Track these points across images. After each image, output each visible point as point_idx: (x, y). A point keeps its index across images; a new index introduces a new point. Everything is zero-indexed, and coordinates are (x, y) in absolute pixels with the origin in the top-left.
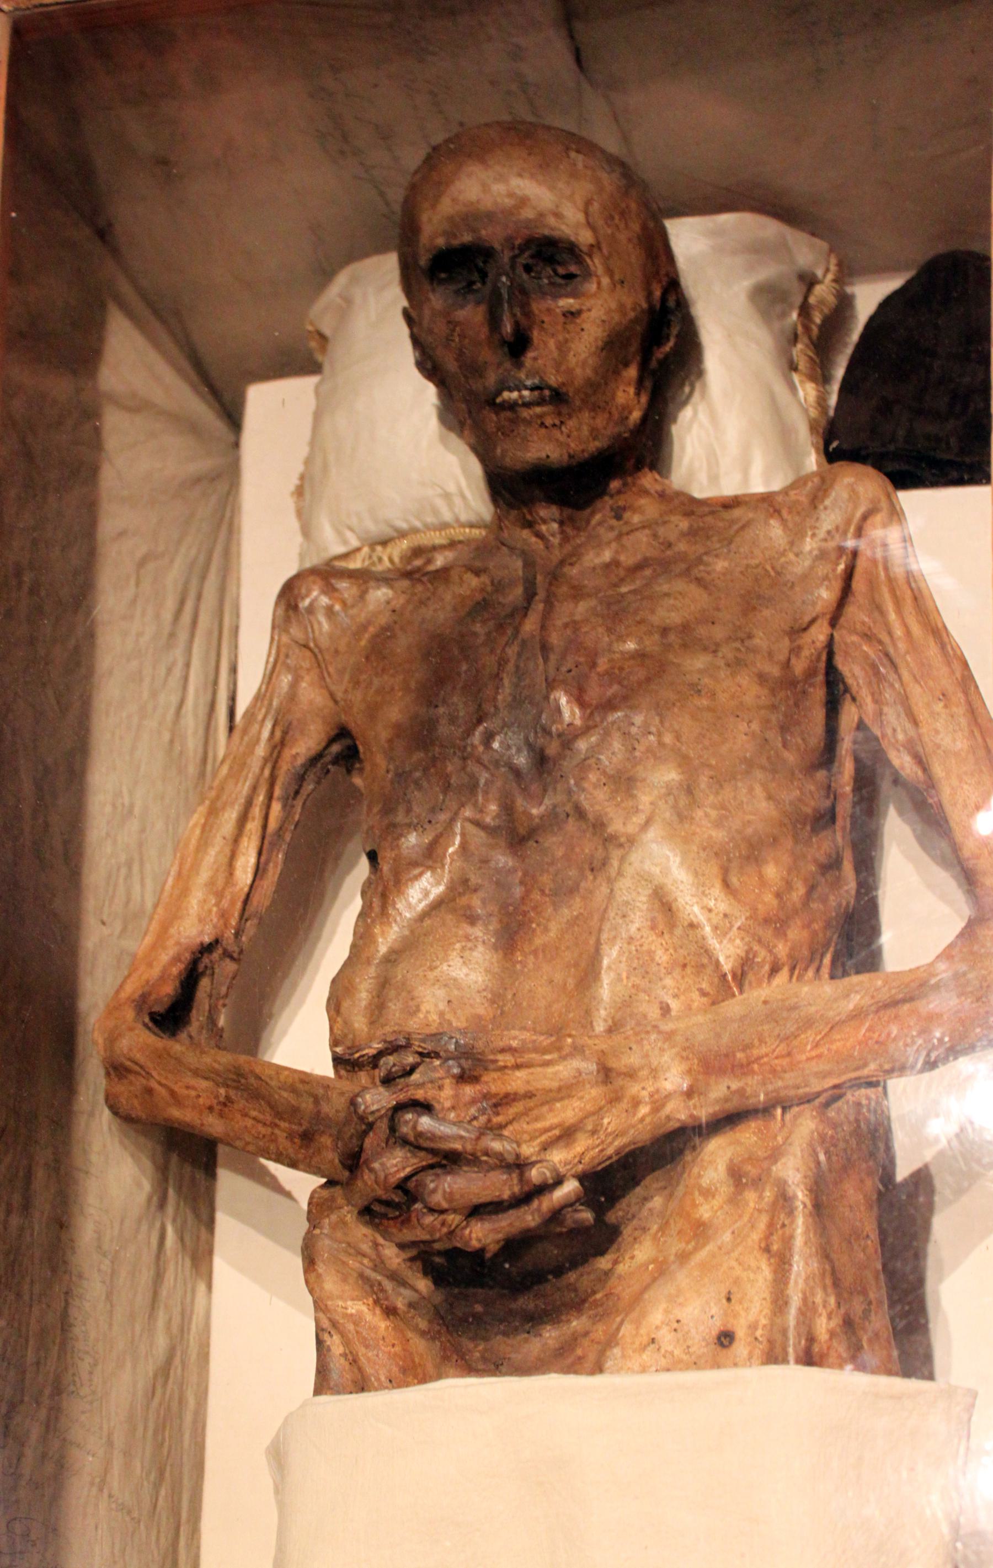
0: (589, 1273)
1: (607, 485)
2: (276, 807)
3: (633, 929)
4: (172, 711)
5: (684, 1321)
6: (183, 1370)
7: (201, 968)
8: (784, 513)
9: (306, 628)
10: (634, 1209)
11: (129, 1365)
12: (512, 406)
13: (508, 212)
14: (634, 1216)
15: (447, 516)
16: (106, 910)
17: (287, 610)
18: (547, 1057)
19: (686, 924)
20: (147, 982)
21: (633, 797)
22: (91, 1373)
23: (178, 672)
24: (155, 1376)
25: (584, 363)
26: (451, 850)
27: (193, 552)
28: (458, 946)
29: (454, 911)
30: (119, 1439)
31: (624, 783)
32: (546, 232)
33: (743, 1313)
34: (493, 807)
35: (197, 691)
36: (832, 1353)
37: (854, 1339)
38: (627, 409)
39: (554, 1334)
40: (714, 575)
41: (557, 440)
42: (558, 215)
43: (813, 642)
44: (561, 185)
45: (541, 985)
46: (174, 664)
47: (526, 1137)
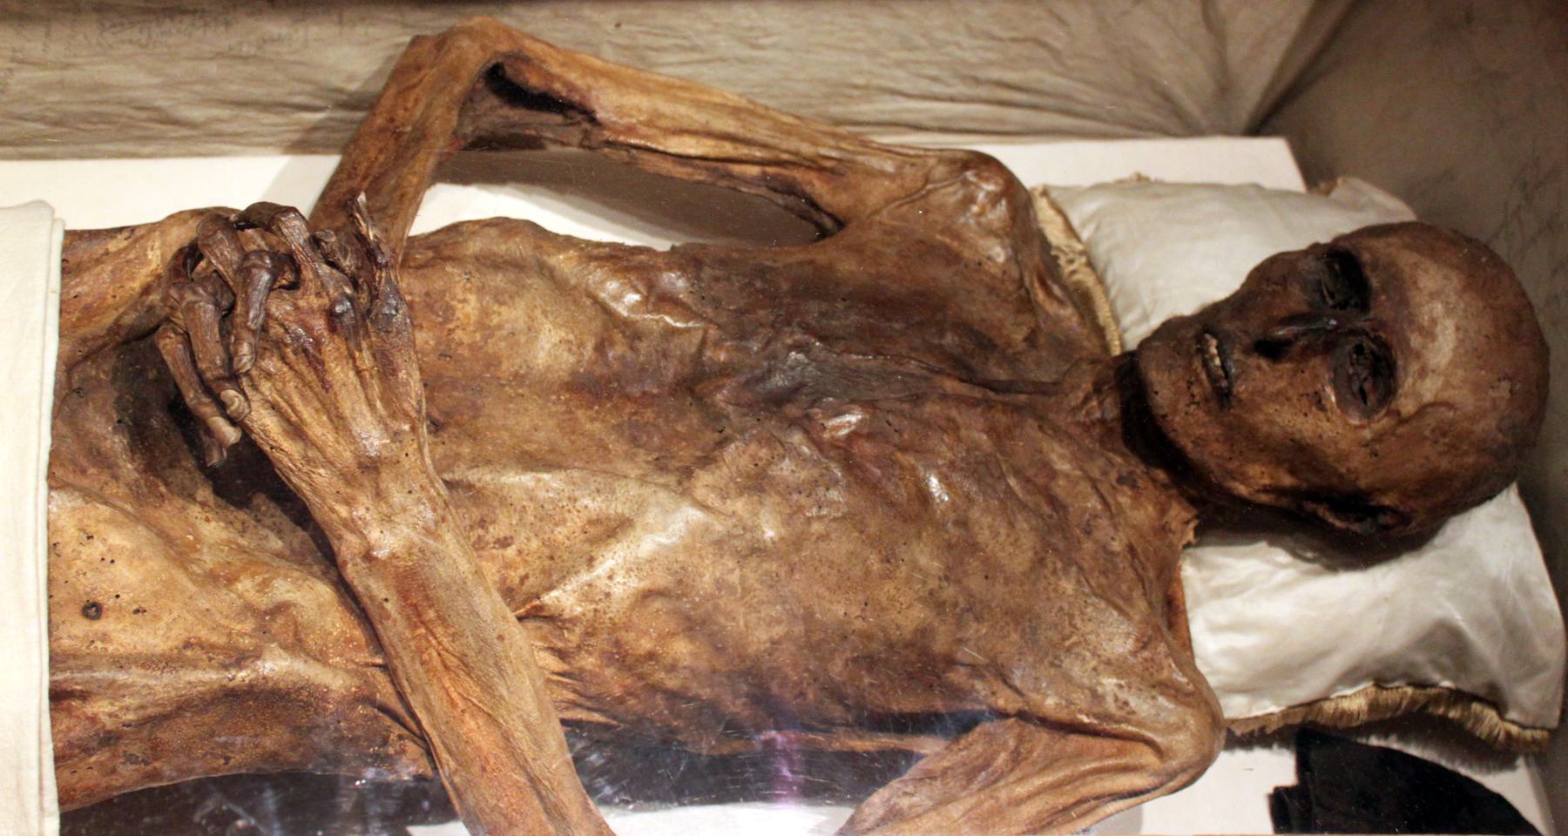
0: (192, 480)
1: (1158, 466)
2: (754, 171)
3: (587, 501)
4: (891, 85)
5: (113, 568)
6: (176, 139)
7: (571, 113)
8: (1146, 654)
10: (268, 521)
11: (157, 80)
12: (1202, 351)
14: (258, 521)
15: (1127, 320)
16: (634, 28)
17: (961, 160)
18: (379, 404)
20: (544, 62)
21: (741, 494)
22: (131, 42)
23: (937, 89)
24: (156, 109)
25: (1272, 423)
26: (668, 319)
27: (1085, 98)
28: (571, 337)
29: (606, 328)
30: (72, 75)
31: (757, 483)
32: (1400, 363)
33: (120, 627)
34: (722, 357)
35: (928, 110)
36: (72, 722)
37: (94, 744)
38: (1244, 479)
39: (118, 447)
40: (1052, 579)
41: (1177, 401)
42: (1423, 373)
43: (994, 693)
44: (1460, 373)
45: (535, 421)
46: (948, 85)
47: (280, 385)
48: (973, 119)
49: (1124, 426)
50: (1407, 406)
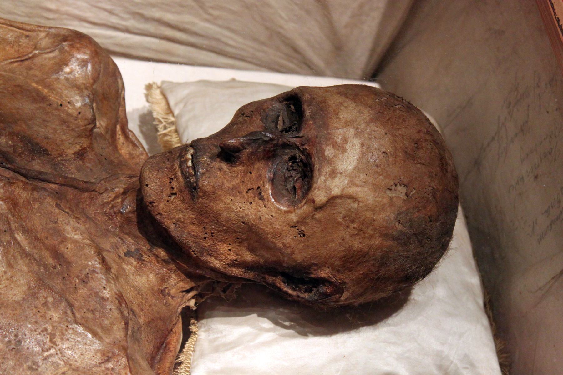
1: (160, 247)
4: (77, 12)
9: (48, 48)
13: (328, 138)
23: (114, 20)
25: (228, 209)
42: (333, 174)
48: (149, 49)
49: (139, 216)
50: (320, 196)
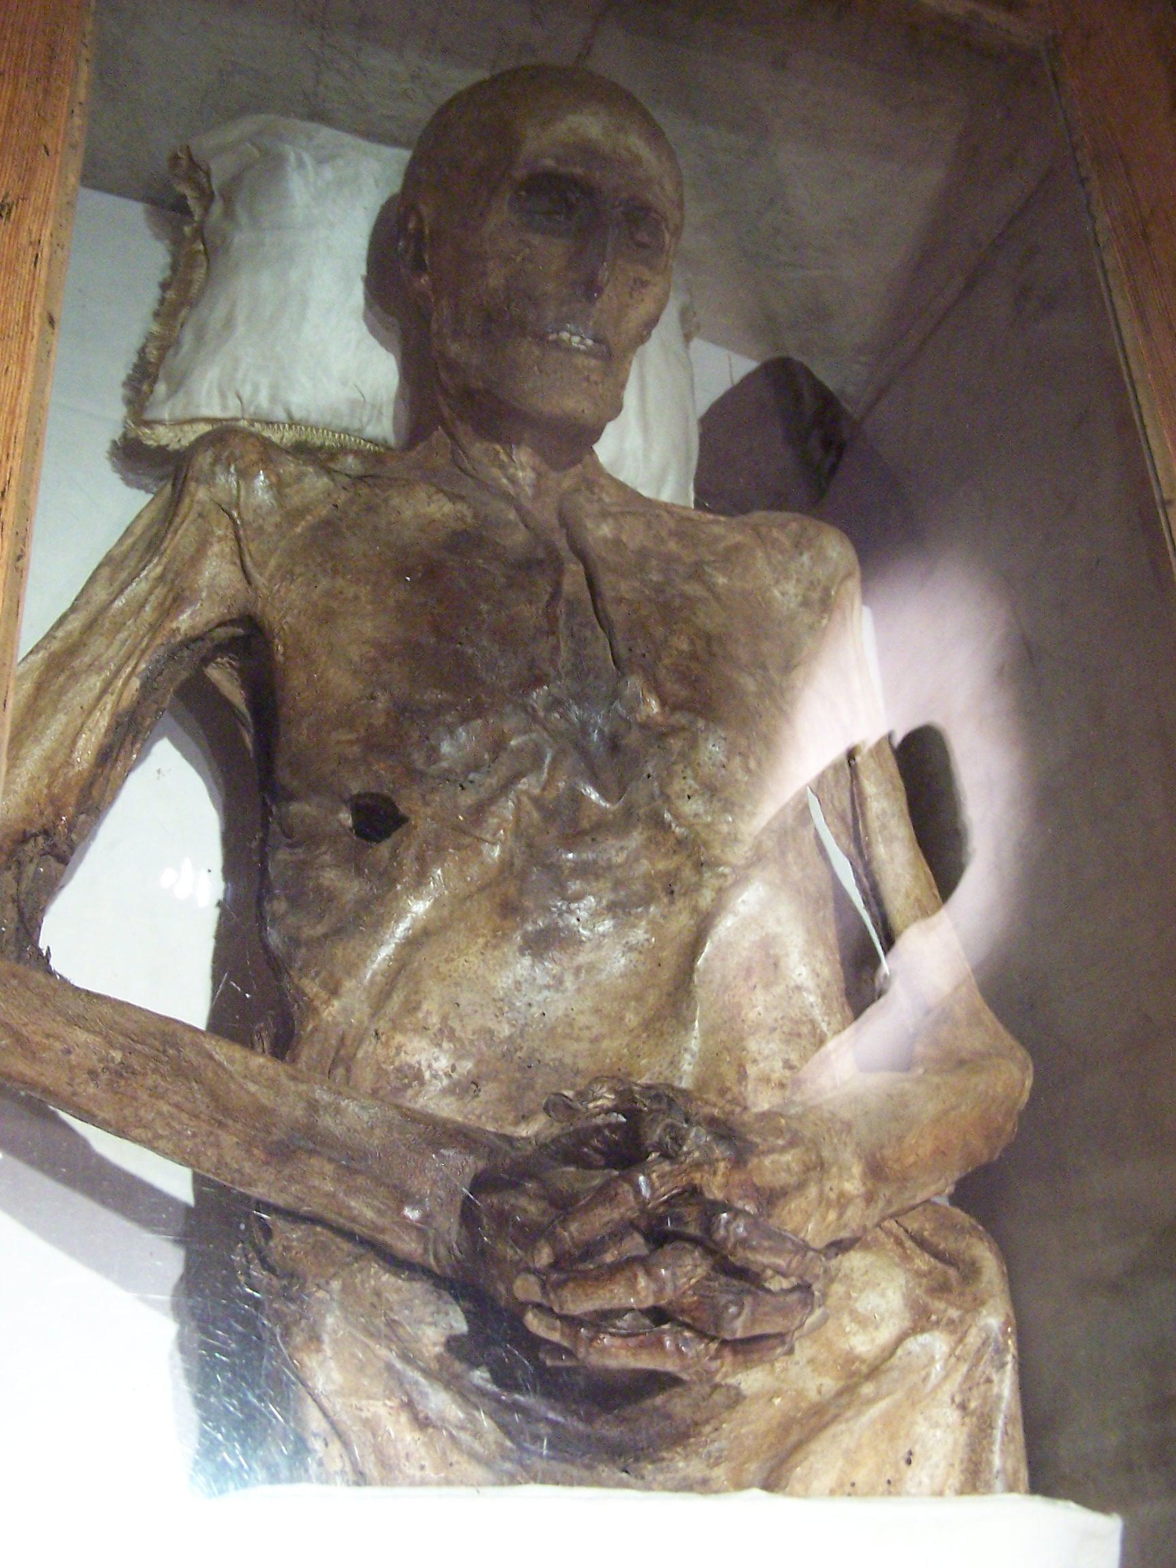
19: (792, 984)
